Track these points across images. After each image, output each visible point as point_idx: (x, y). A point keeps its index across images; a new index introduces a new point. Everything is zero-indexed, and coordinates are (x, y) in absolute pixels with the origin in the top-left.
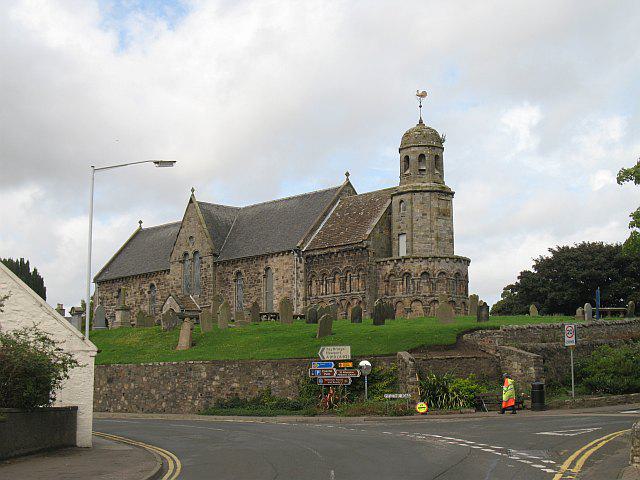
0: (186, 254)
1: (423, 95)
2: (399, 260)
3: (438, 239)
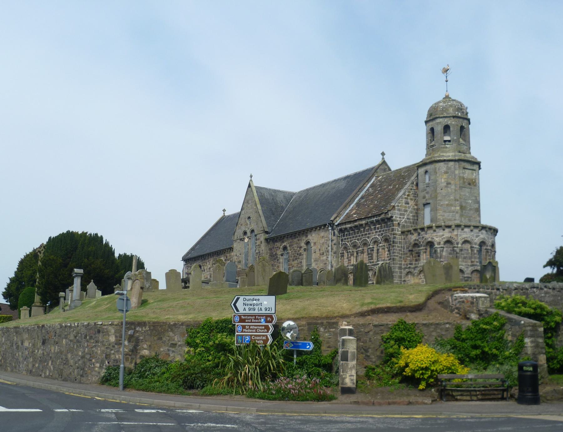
0: (245, 233)
1: (446, 71)
2: (423, 229)
3: (462, 208)
